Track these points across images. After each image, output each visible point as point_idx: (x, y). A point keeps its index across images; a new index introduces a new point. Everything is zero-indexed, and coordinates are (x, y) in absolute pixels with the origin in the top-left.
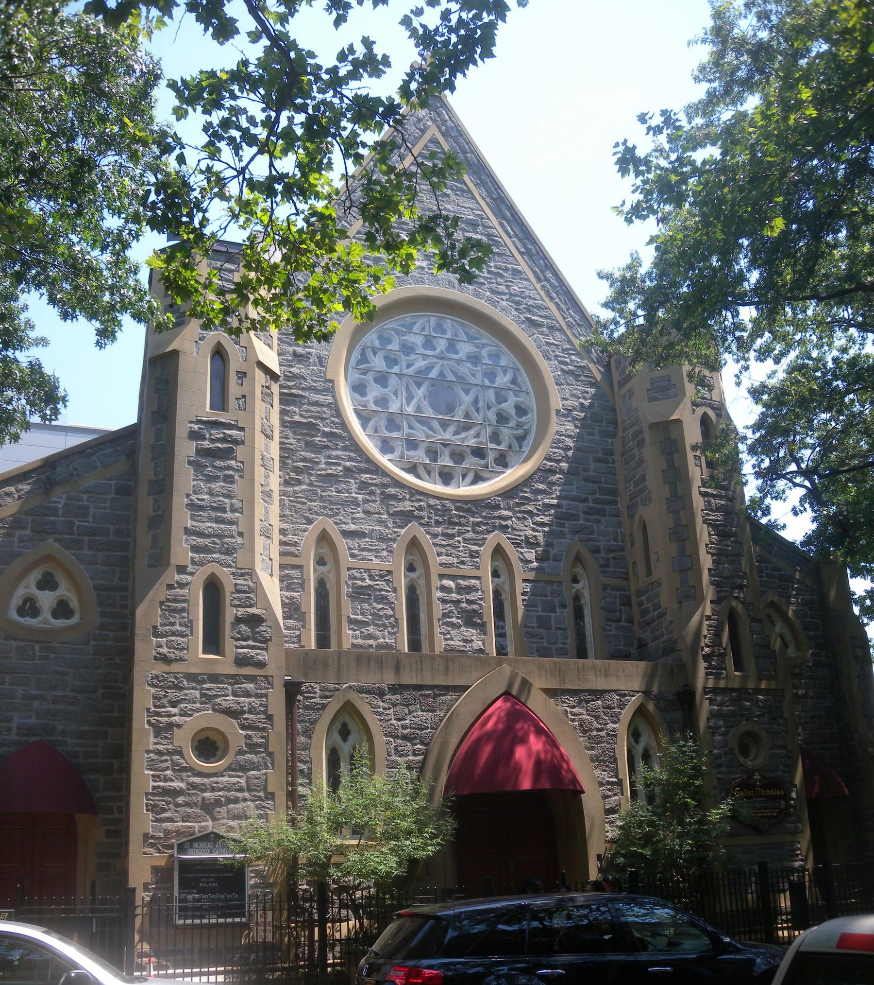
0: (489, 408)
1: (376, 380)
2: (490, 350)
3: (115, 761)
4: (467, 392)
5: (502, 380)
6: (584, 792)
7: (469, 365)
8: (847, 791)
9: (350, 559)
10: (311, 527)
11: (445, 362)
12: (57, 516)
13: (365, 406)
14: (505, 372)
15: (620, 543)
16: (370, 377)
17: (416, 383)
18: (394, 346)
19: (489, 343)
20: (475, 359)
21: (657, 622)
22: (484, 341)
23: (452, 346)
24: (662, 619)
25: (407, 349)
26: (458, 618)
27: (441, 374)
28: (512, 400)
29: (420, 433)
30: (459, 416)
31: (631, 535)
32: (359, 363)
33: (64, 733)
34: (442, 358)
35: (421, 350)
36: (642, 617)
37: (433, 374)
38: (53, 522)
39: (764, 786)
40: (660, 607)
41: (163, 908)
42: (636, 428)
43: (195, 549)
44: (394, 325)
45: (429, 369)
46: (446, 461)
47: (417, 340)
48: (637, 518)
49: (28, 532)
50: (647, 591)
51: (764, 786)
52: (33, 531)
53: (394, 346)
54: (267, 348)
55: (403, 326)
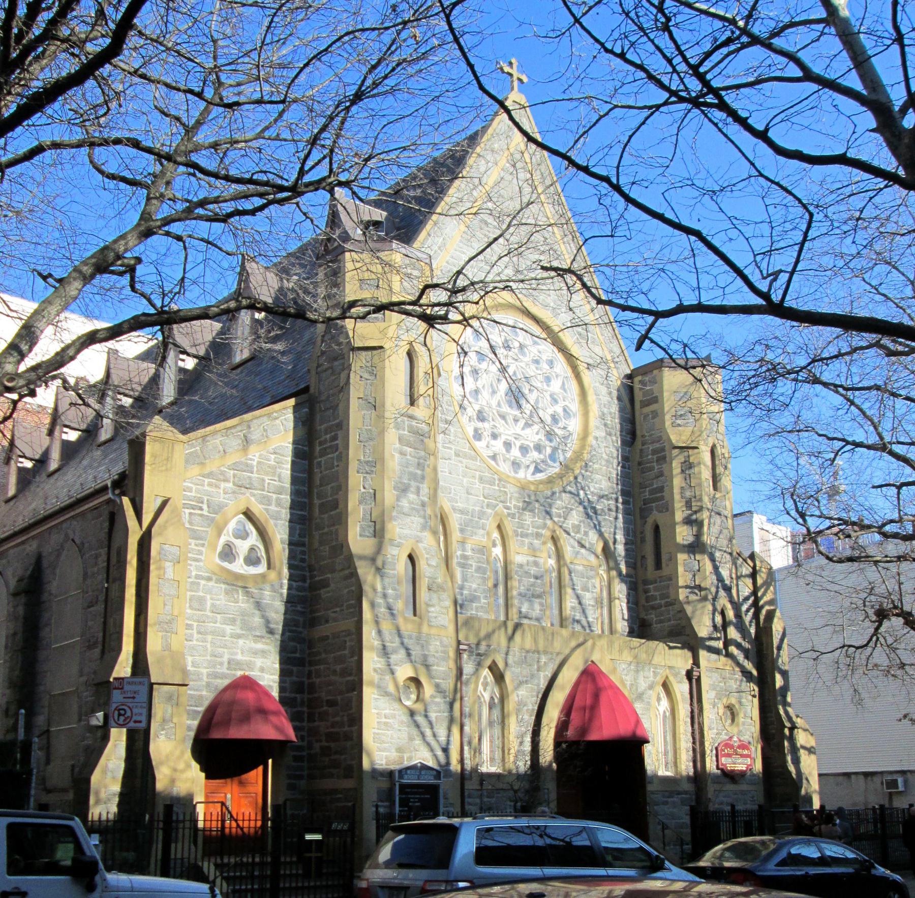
3: (297, 695)
5: (556, 386)
6: (648, 742)
8: (19, 756)
12: (252, 473)
21: (663, 609)
24: (670, 608)
26: (191, 565)
28: (562, 404)
31: (642, 533)
33: (262, 670)
36: (647, 602)
38: (250, 478)
39: (739, 747)
40: (668, 597)
42: (657, 445)
48: (650, 521)
49: (231, 485)
50: (655, 582)
51: (739, 747)
52: (234, 484)
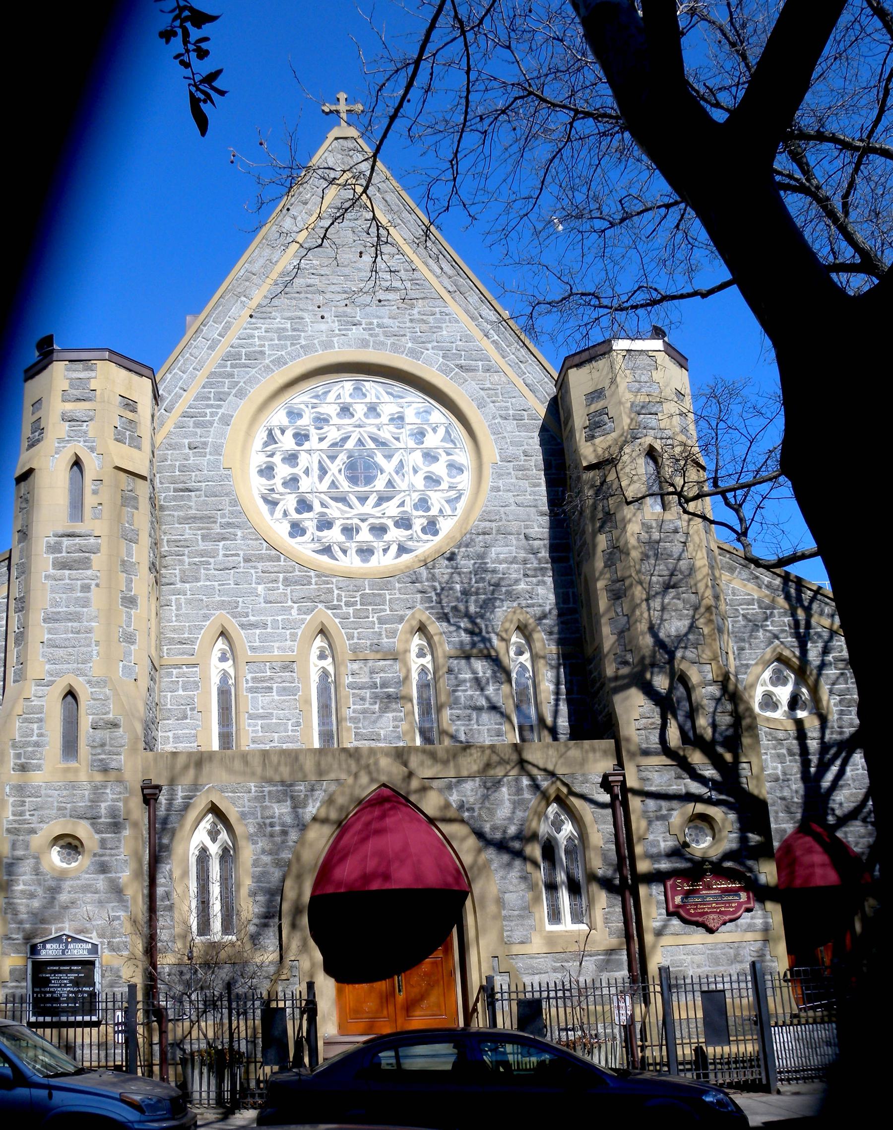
0: (415, 471)
1: (284, 460)
2: (416, 409)
4: (389, 457)
7: (392, 428)
9: (249, 653)
10: (208, 623)
11: (361, 430)
13: (273, 490)
14: (434, 430)
15: (571, 605)
16: (277, 459)
17: (329, 457)
18: (306, 421)
19: (415, 400)
20: (399, 419)
22: (409, 399)
23: (373, 409)
25: (321, 421)
27: (360, 442)
29: (335, 510)
30: (380, 484)
32: (266, 444)
34: (360, 426)
35: (335, 420)
37: (350, 444)
41: (734, 1066)
43: (52, 661)
44: (305, 398)
45: (345, 439)
46: (364, 535)
47: (330, 409)
53: (306, 421)
54: (136, 451)
55: (317, 397)
